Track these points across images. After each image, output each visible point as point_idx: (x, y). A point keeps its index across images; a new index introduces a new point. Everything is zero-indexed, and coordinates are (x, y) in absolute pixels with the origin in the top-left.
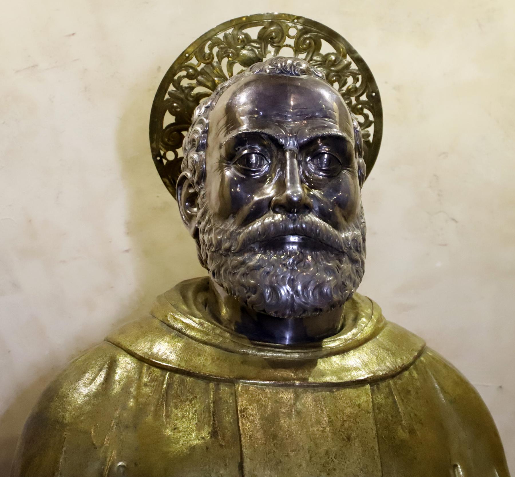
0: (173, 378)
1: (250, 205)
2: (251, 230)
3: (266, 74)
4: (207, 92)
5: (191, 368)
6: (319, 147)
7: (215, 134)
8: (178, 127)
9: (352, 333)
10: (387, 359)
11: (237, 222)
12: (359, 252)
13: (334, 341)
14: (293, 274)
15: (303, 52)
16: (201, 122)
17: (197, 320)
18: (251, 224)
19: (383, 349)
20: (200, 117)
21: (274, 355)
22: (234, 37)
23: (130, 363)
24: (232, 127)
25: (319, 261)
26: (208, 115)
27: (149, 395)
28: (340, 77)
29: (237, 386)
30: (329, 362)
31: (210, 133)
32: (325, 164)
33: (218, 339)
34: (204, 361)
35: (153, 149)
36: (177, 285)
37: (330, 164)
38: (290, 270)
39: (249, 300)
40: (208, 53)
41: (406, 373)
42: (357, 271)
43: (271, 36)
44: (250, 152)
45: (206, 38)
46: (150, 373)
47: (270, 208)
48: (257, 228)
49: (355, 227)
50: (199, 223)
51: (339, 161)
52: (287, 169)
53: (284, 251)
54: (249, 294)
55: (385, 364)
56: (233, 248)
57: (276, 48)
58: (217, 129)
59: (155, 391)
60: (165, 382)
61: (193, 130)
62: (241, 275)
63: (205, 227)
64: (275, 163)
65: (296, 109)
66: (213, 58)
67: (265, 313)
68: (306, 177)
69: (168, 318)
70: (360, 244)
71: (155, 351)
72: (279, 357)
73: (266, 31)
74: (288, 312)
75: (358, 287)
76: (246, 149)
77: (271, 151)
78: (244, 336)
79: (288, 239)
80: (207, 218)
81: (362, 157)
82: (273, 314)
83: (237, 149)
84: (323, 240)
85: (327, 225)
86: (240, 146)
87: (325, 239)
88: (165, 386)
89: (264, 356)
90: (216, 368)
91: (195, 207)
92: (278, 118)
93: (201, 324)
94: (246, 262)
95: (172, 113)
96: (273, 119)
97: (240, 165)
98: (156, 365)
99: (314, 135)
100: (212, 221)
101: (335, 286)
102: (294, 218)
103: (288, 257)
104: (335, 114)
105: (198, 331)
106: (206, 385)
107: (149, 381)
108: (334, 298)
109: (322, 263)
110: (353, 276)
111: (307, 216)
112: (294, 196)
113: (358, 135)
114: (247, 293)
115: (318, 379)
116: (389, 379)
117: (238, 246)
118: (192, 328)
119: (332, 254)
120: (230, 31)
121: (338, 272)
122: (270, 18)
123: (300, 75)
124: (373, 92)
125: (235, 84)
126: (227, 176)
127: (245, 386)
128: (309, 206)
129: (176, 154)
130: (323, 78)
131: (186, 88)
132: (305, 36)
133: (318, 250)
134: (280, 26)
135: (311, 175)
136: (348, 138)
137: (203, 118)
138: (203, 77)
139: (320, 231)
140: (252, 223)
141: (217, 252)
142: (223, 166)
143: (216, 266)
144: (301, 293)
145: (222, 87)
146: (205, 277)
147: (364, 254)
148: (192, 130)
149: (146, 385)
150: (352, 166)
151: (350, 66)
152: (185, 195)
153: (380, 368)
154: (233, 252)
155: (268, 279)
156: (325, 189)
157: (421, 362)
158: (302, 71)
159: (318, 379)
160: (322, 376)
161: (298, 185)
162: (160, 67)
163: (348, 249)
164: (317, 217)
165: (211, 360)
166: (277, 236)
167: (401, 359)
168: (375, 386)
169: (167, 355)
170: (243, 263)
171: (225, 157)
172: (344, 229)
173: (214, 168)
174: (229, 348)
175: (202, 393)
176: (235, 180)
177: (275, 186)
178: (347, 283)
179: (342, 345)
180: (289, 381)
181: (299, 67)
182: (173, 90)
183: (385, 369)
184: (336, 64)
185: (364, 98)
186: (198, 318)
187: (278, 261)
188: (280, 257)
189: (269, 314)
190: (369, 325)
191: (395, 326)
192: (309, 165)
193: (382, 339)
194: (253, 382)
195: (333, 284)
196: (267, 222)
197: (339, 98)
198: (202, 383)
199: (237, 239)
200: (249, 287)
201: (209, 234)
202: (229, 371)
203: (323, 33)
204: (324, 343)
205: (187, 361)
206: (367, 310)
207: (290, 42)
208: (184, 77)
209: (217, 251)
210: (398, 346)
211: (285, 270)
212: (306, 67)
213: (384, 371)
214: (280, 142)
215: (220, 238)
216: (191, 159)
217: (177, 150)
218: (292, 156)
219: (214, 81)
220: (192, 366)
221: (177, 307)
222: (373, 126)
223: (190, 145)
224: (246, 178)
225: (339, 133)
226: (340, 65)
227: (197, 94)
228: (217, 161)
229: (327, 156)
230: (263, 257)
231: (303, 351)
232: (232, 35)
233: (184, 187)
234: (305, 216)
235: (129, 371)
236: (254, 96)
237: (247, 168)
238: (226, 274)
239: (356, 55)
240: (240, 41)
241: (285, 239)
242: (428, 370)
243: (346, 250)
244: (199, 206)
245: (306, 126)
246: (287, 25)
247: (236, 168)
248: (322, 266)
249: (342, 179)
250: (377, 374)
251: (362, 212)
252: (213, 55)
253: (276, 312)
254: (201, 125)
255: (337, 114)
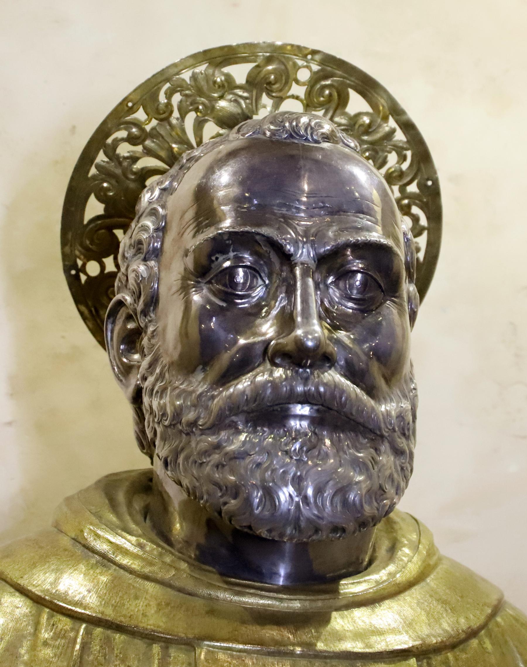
0: (91, 634)
1: (235, 349)
2: (233, 392)
3: (265, 138)
4: (160, 167)
5: (123, 619)
6: (349, 262)
7: (177, 234)
8: (108, 221)
9: (388, 572)
10: (444, 618)
11: (209, 379)
12: (407, 438)
13: (359, 583)
14: (301, 468)
15: (318, 109)
16: (153, 213)
17: (133, 539)
18: (232, 383)
19: (438, 600)
20: (151, 204)
21: (262, 602)
22: (207, 77)
23: (20, 606)
24: (207, 221)
25: (343, 448)
26: (165, 202)
27: (51, 662)
28: (377, 152)
29: (198, 651)
30: (351, 617)
31: (168, 232)
32: (358, 289)
33: (168, 571)
34: (144, 608)
35: (65, 256)
36: (99, 481)
37: (365, 290)
38: (295, 462)
39: (224, 508)
40: (164, 103)
41: (474, 642)
42: (402, 468)
43: (268, 81)
44: (233, 265)
45: (163, 78)
46: (53, 625)
47: (266, 358)
48: (243, 389)
49: (401, 396)
50: (144, 379)
51: (380, 286)
52: (297, 295)
53: (286, 429)
54: (225, 499)
55: (440, 625)
56: (200, 422)
57: (275, 99)
58: (181, 224)
59: (61, 655)
60: (79, 640)
61: (140, 225)
62: (213, 466)
63: (154, 385)
64: (276, 285)
65: (313, 197)
66: (172, 112)
67: (251, 532)
68: (326, 310)
69: (85, 534)
70: (408, 424)
71: (62, 587)
72: (269, 605)
73: (260, 72)
74: (289, 531)
75: (403, 496)
76: (228, 260)
77: (269, 263)
78: (210, 568)
79: (293, 409)
80: (158, 371)
81: (413, 282)
82: (264, 533)
83: (214, 258)
84: (351, 414)
85: (358, 390)
86: (220, 255)
87: (354, 413)
88: (78, 647)
89: (245, 603)
90: (164, 619)
91: (136, 353)
92: (284, 211)
93: (141, 546)
94: (222, 445)
95: (100, 199)
96: (276, 211)
97: (217, 284)
98: (64, 611)
99: (342, 240)
100: (167, 375)
101: (368, 491)
102: (305, 375)
103: (293, 439)
104: (376, 208)
105: (135, 556)
106: (147, 647)
107: (52, 638)
108: (364, 510)
109: (347, 453)
110: (395, 476)
111: (326, 373)
112: (308, 339)
113: (409, 246)
114: (221, 497)
115: (332, 645)
116: (447, 651)
117: (209, 418)
118: (126, 552)
119: (365, 438)
120: (202, 68)
121: (374, 469)
122: (269, 50)
123: (320, 143)
124: (428, 179)
125: (210, 153)
126: (195, 301)
127: (213, 652)
128: (330, 357)
129: (103, 267)
130: (356, 151)
131: (125, 158)
132: (323, 83)
133: (343, 431)
134: (283, 64)
135: (334, 307)
136: (396, 249)
137: (155, 206)
138: (153, 142)
139: (346, 399)
140: (235, 382)
141: (174, 427)
142: (188, 285)
143: (170, 451)
144: (312, 500)
145: (188, 158)
146: (144, 469)
147: (413, 441)
148: (136, 226)
149: (46, 644)
150: (400, 294)
151: (394, 136)
152: (119, 334)
153: (433, 632)
154: (201, 427)
155: (258, 474)
156: (359, 329)
157: (498, 625)
158: (324, 136)
159: (332, 645)
160: (339, 641)
161: (315, 321)
162: (74, 127)
163: (390, 432)
164: (341, 375)
165: (155, 607)
166: (277, 405)
167: (467, 618)
168: (425, 661)
169: (81, 595)
170: (218, 447)
171: (192, 270)
172: (384, 398)
173: (174, 289)
174: (186, 588)
175: (139, 660)
176: (209, 310)
177: (275, 321)
178: (387, 487)
179: (371, 590)
180: (284, 646)
181: (320, 129)
182: (104, 161)
183: (440, 634)
184: (370, 130)
185: (413, 188)
186: (135, 536)
187: (276, 445)
188: (279, 440)
189: (258, 532)
190: (415, 559)
191: (455, 564)
192: (331, 291)
193: (434, 584)
194: (225, 645)
195: (364, 487)
196: (260, 381)
197: (381, 182)
198: (140, 644)
199: (207, 406)
200: (226, 487)
201: (161, 398)
202: (186, 626)
203: (353, 79)
204: (343, 587)
205: (116, 607)
206: (411, 536)
207: (299, 90)
208: (123, 140)
209: (174, 425)
210: (462, 597)
211: (288, 460)
212: (330, 129)
213: (439, 637)
214: (287, 250)
215: (179, 405)
216: (135, 273)
217: (104, 260)
218: (305, 273)
219: (172, 148)
220: (125, 616)
221: (100, 517)
222: (425, 234)
223: (132, 250)
224: (226, 307)
225: (382, 240)
226: (377, 132)
227: (143, 169)
228: (179, 276)
229: (362, 276)
230: (252, 437)
231: (308, 598)
232: (204, 75)
233: (119, 319)
234: (323, 373)
235: (17, 620)
236: (245, 174)
237: (230, 290)
238: (188, 462)
239: (404, 118)
240: (216, 86)
241: (288, 409)
242: (508, 639)
243: (387, 432)
244: (145, 350)
245: (330, 225)
246: (295, 64)
247: (210, 290)
248: (347, 457)
249: (384, 316)
250: (428, 641)
251: (411, 373)
252: (172, 106)
253: (270, 531)
254: (153, 218)
255: (378, 209)
